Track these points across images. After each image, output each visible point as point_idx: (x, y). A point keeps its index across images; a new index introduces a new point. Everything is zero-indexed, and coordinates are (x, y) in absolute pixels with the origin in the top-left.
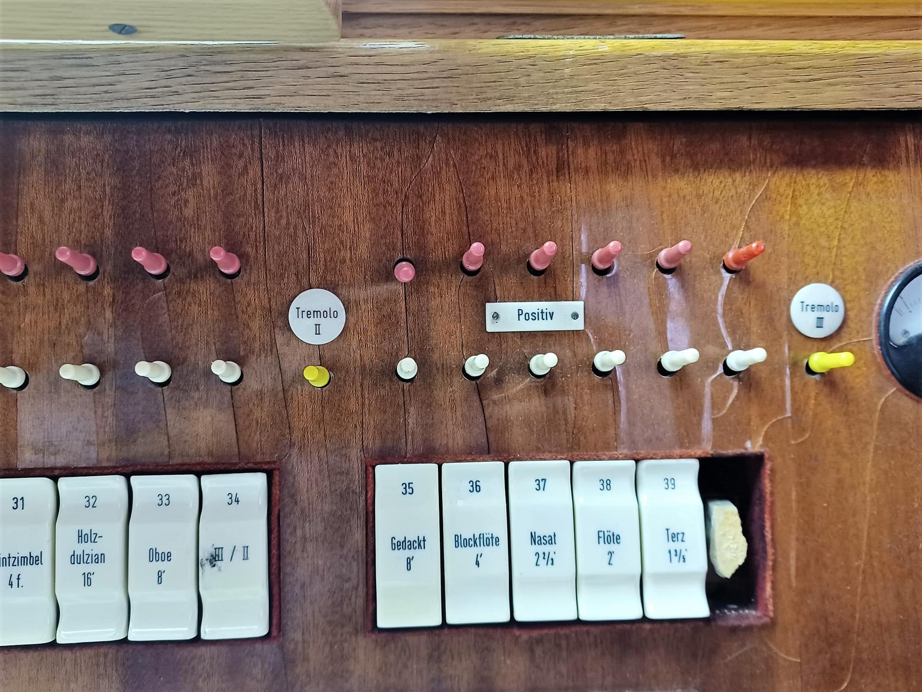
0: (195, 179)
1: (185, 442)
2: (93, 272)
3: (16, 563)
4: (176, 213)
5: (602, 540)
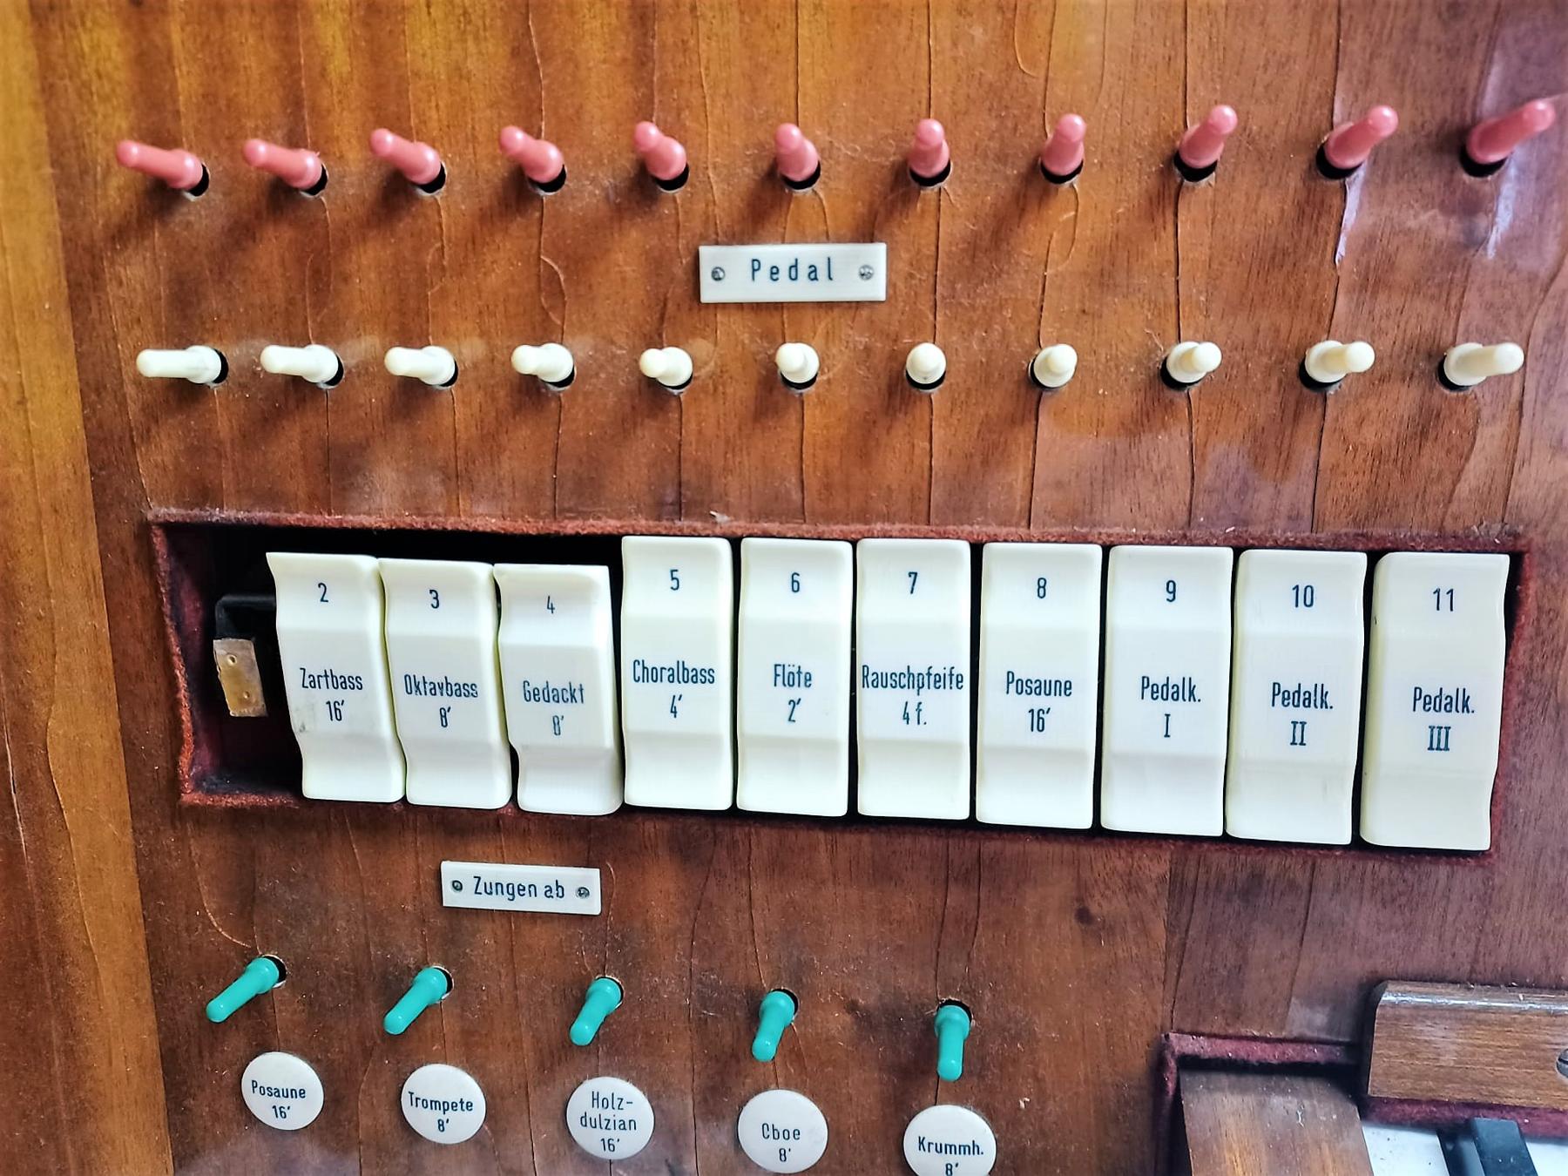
5: (780, 679)
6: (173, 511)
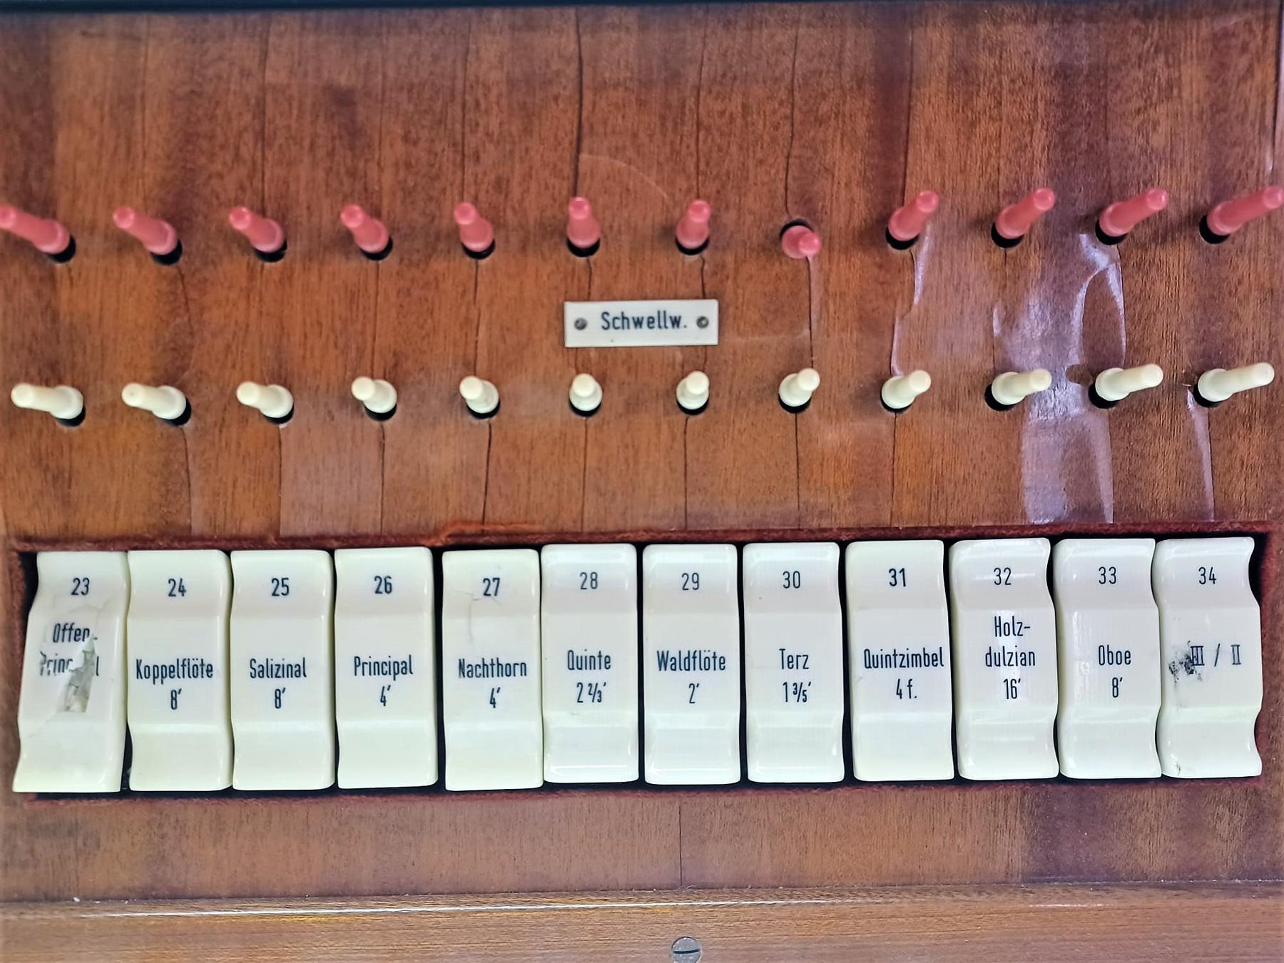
0: (1170, 89)
1: (1137, 490)
2: (479, 251)
3: (905, 663)
4: (1141, 141)
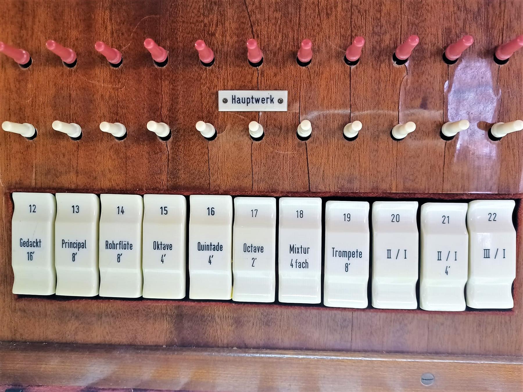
6: (49, 222)
